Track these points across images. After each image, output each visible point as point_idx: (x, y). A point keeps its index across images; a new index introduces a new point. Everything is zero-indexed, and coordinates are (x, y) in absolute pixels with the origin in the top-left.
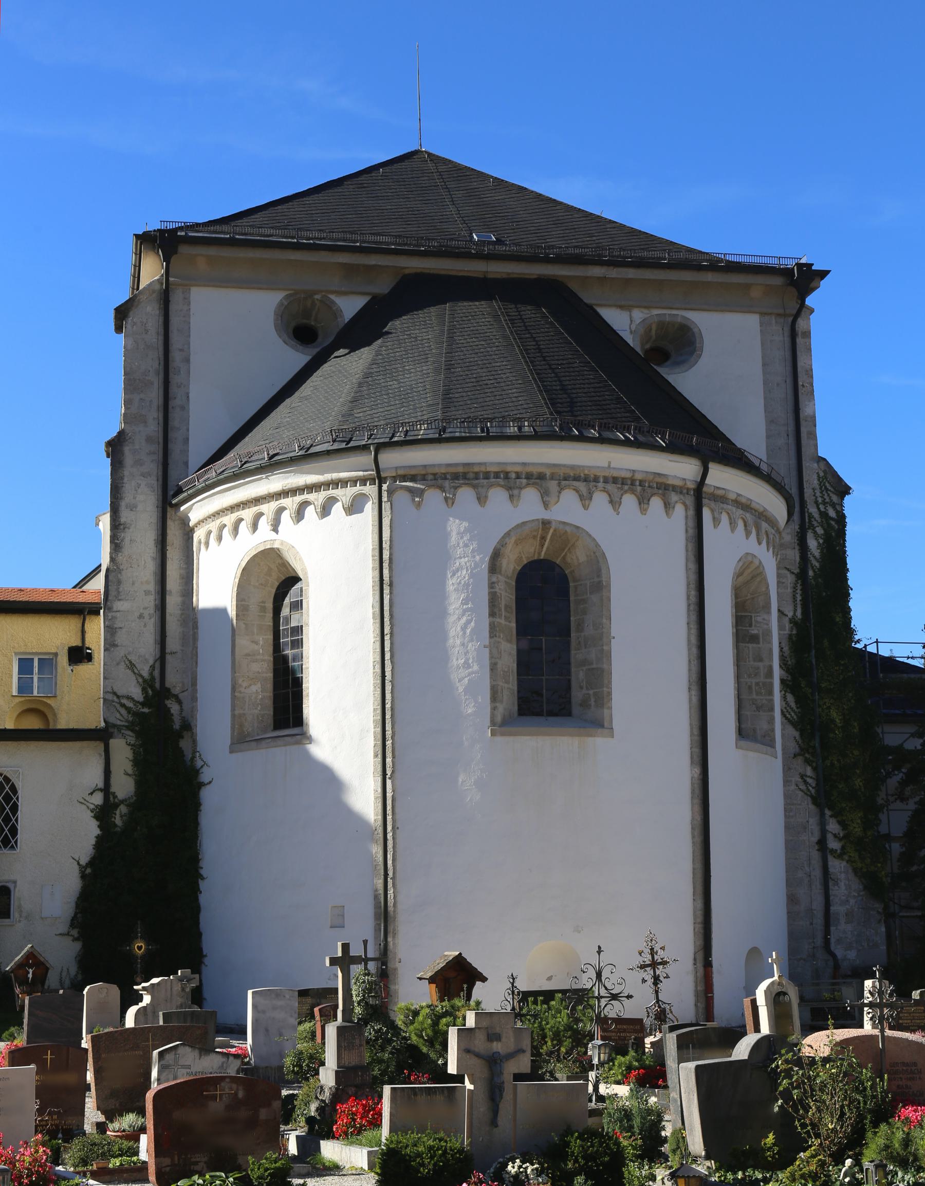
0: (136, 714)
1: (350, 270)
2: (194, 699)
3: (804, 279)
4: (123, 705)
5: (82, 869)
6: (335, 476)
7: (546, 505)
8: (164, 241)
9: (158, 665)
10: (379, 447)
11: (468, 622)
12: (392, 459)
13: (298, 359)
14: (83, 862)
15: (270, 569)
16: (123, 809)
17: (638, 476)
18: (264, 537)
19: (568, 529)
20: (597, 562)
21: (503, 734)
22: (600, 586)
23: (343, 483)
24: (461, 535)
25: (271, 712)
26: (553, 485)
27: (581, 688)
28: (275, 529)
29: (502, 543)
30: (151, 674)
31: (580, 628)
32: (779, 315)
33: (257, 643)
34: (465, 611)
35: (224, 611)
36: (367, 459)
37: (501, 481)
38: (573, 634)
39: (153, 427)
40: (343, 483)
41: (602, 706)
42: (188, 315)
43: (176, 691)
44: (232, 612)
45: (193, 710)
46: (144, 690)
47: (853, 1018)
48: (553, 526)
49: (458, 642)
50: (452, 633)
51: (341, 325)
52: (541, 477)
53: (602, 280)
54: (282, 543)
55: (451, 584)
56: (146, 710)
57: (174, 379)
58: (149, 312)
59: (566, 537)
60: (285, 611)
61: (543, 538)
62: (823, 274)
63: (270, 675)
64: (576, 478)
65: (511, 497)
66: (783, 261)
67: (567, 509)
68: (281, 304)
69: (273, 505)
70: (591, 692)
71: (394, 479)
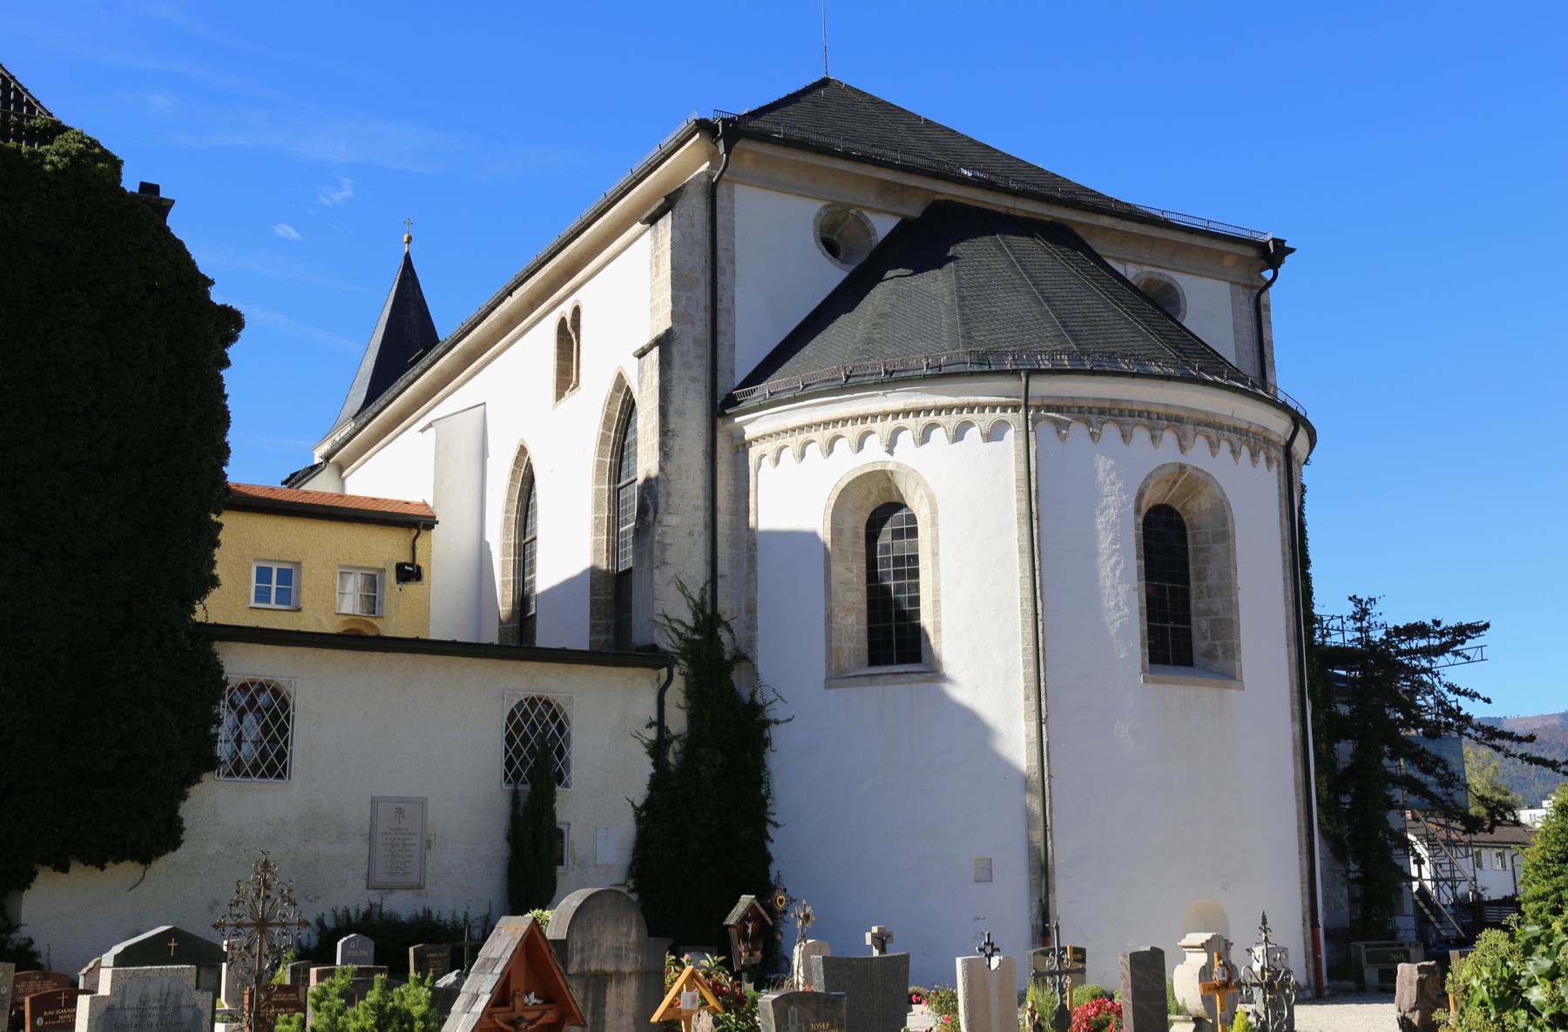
0: (687, 641)
1: (886, 188)
2: (752, 626)
3: (1273, 254)
4: (674, 630)
5: (638, 811)
6: (972, 399)
7: (1183, 449)
8: (727, 133)
9: (708, 588)
10: (1031, 373)
11: (1117, 564)
12: (1043, 387)
13: (832, 275)
14: (638, 803)
15: (870, 492)
16: (676, 746)
17: (1253, 429)
18: (874, 456)
19: (1201, 475)
20: (1222, 512)
21: (1153, 682)
22: (1224, 535)
23: (949, 409)
24: (1108, 473)
25: (865, 646)
26: (1189, 429)
27: (1205, 638)
28: (890, 451)
29: (1145, 484)
30: (702, 598)
31: (1201, 576)
32: (1245, 286)
33: (851, 571)
34: (1114, 552)
35: (812, 536)
36: (1014, 386)
37: (1145, 421)
38: (1192, 583)
39: (701, 329)
40: (949, 409)
41: (1233, 657)
42: (732, 213)
43: (726, 618)
44: (825, 534)
45: (751, 642)
46: (695, 614)
47: (1371, 975)
48: (1189, 471)
49: (1108, 583)
50: (1103, 573)
51: (875, 244)
52: (1179, 420)
53: (1105, 230)
54: (899, 465)
55: (1101, 522)
56: (697, 637)
57: (721, 280)
58: (694, 204)
59: (1188, 480)
60: (885, 538)
61: (1175, 482)
62: (1292, 250)
63: (864, 606)
64: (1208, 425)
65: (1153, 438)
66: (1255, 235)
67: (1199, 455)
68: (819, 214)
69: (890, 424)
70: (1218, 643)
71: (1038, 409)
